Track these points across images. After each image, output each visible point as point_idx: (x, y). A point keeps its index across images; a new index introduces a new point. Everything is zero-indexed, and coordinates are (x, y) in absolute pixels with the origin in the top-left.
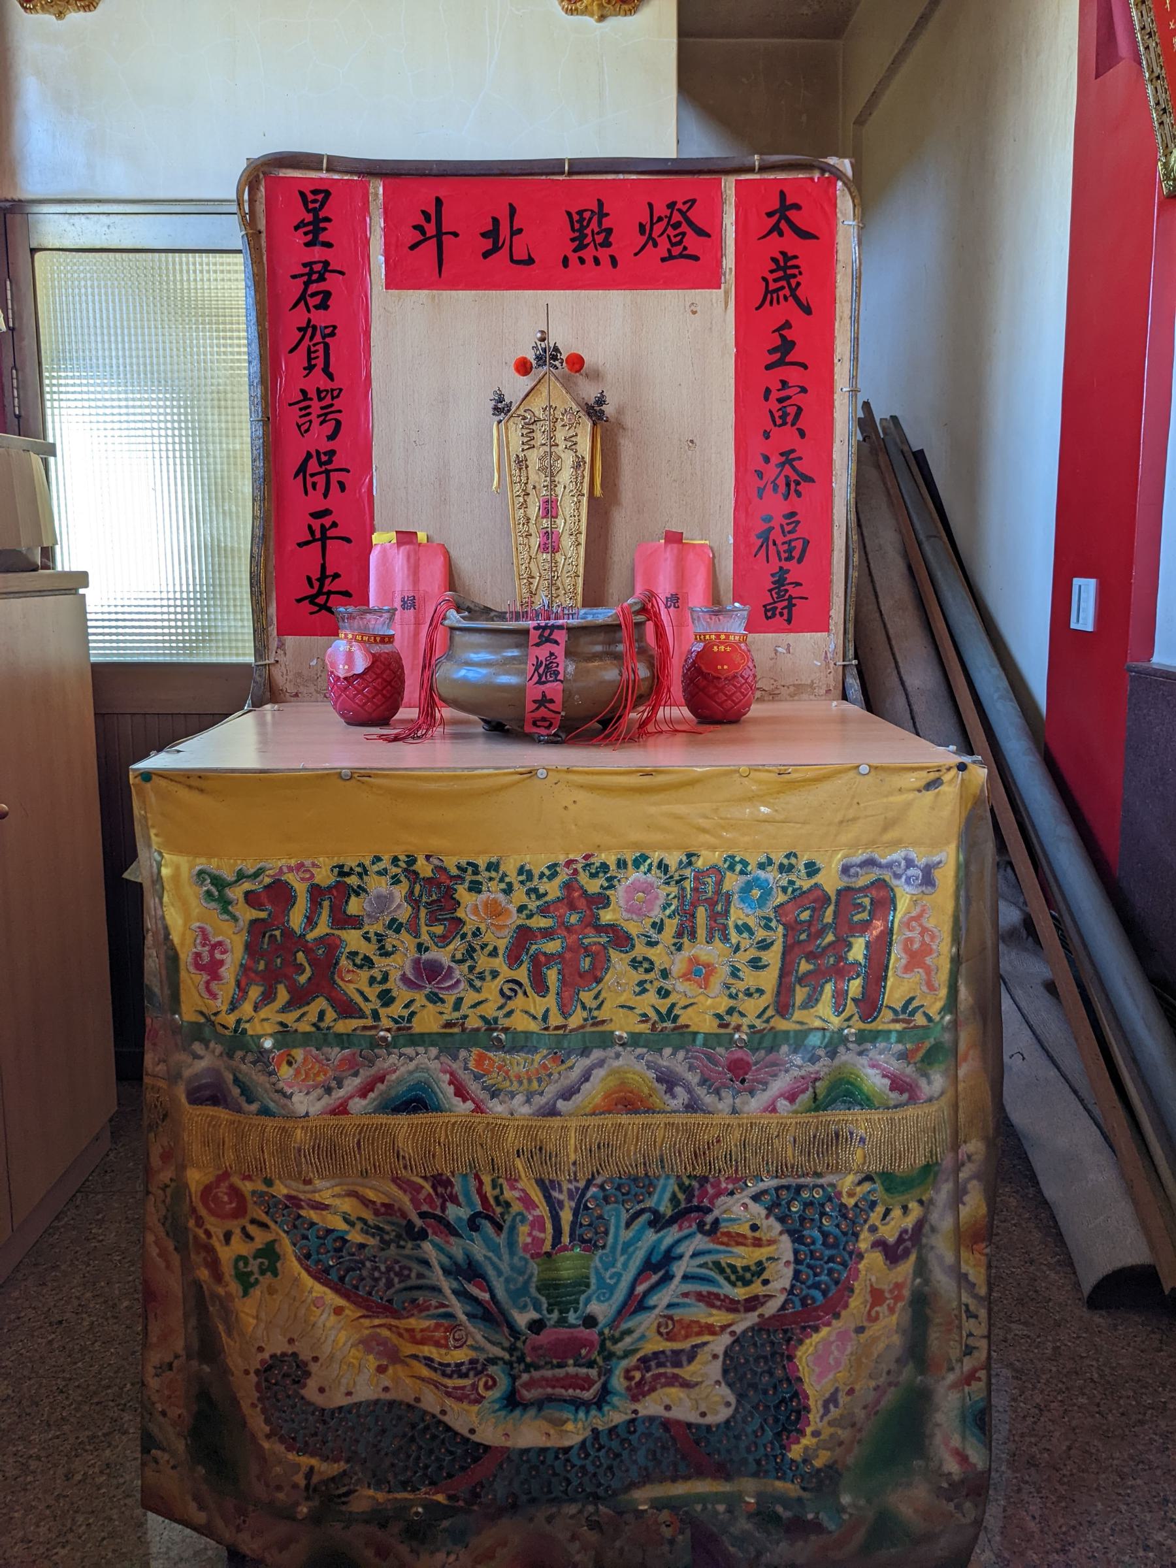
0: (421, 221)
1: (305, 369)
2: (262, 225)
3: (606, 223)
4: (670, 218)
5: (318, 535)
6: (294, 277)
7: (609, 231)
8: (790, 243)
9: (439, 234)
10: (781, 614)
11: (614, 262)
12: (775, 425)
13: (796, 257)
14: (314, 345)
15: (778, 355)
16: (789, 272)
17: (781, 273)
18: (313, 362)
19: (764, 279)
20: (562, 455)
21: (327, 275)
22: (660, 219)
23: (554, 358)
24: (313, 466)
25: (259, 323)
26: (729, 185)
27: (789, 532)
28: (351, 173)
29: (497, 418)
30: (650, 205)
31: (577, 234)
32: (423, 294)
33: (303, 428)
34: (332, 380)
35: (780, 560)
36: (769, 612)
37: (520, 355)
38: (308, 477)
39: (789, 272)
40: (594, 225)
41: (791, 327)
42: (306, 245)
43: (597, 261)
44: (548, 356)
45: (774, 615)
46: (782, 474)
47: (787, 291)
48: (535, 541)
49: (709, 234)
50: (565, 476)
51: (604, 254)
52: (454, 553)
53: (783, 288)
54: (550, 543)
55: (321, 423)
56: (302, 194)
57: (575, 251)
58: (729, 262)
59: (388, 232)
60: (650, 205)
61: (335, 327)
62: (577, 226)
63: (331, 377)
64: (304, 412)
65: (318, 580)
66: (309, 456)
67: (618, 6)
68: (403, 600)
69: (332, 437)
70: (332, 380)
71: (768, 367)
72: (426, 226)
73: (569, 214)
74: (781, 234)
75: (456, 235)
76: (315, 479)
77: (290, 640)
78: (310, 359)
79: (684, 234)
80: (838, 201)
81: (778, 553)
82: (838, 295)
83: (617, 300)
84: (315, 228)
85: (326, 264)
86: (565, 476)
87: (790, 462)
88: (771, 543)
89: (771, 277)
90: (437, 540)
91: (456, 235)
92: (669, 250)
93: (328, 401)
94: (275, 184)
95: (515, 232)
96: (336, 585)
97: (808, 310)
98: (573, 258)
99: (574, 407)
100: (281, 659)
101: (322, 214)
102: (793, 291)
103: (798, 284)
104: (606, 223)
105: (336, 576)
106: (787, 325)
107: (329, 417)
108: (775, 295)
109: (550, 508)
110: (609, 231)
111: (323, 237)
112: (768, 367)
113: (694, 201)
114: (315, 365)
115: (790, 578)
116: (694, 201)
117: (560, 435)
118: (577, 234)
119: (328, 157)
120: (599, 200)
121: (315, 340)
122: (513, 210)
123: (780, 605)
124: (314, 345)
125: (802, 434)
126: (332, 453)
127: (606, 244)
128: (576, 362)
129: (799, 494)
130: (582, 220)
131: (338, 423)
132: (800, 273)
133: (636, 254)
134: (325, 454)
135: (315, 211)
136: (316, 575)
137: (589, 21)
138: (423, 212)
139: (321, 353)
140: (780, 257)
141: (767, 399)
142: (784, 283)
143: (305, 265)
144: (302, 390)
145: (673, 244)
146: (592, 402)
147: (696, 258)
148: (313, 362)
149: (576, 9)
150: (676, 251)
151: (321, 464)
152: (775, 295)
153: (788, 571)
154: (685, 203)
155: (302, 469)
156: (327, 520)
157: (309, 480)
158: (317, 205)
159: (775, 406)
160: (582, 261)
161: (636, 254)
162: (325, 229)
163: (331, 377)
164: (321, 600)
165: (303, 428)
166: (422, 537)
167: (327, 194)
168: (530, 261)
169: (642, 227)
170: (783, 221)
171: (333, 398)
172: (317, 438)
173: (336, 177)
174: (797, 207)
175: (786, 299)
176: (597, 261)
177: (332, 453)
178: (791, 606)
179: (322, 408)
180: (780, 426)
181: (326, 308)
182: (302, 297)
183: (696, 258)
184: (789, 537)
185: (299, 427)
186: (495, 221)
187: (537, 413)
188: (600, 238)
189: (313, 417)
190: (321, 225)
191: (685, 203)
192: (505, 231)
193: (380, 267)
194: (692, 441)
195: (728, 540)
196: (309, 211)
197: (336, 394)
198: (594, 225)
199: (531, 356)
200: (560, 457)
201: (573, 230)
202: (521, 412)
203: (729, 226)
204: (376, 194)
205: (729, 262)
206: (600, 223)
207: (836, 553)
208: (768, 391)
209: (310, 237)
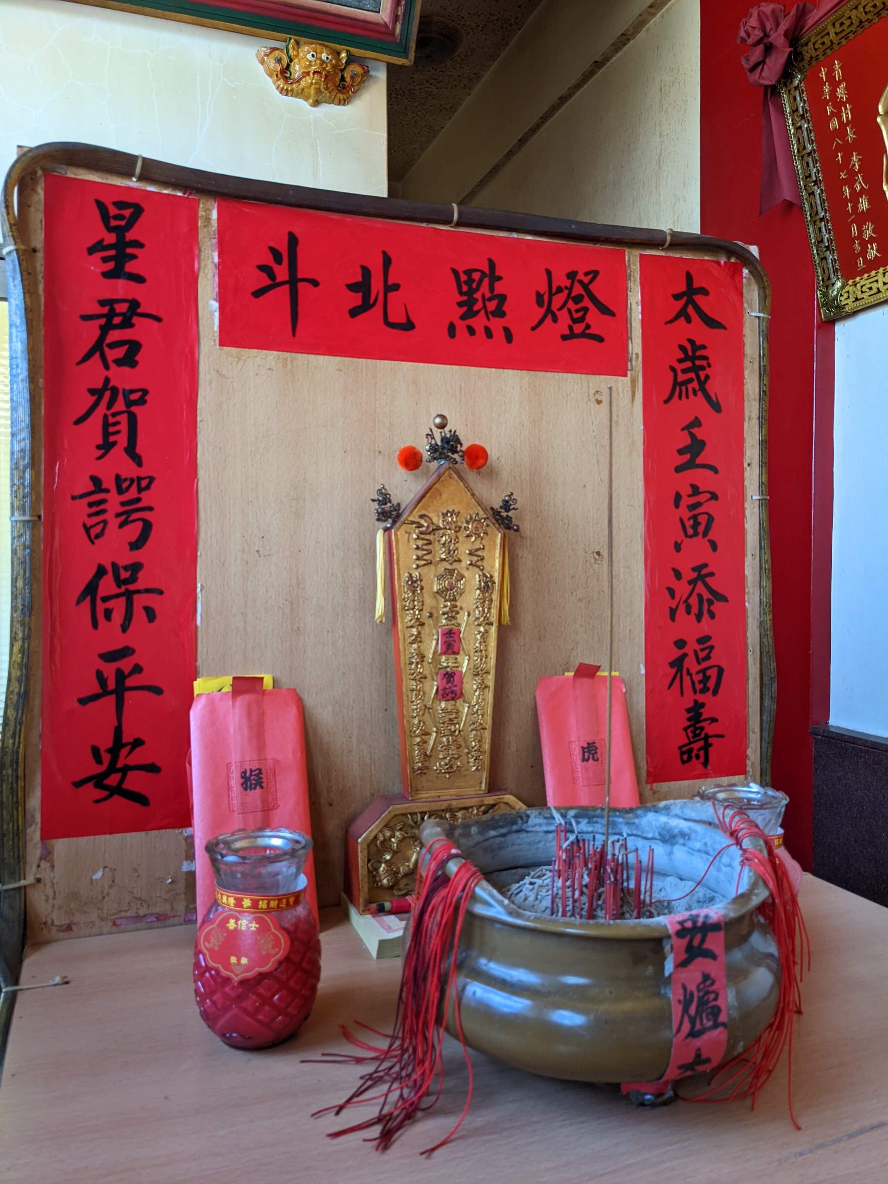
0: (269, 260)
1: (98, 447)
2: (38, 239)
3: (499, 288)
4: (571, 289)
5: (112, 685)
6: (86, 318)
7: (502, 298)
8: (697, 330)
9: (293, 282)
10: (698, 757)
11: (509, 337)
12: (686, 535)
13: (704, 347)
14: (114, 415)
15: (688, 456)
16: (697, 363)
17: (688, 364)
18: (112, 439)
19: (672, 369)
20: (466, 573)
21: (135, 320)
22: (560, 290)
23: (454, 450)
24: (107, 586)
25: (32, 378)
26: (633, 258)
27: (704, 659)
28: (175, 186)
29: (383, 525)
30: (548, 272)
31: (465, 298)
32: (271, 356)
33: (94, 532)
34: (140, 464)
35: (695, 692)
36: (686, 755)
37: (408, 444)
38: (99, 601)
39: (697, 363)
40: (485, 288)
41: (700, 425)
42: (105, 275)
43: (489, 333)
44: (448, 447)
45: (690, 759)
46: (695, 594)
47: (695, 384)
48: (432, 687)
49: (614, 311)
50: (470, 598)
51: (496, 324)
52: (309, 700)
53: (691, 380)
54: (451, 688)
55: (122, 525)
56: (100, 205)
57: (463, 318)
58: (636, 346)
59: (224, 270)
60: (548, 272)
61: (145, 392)
62: (465, 288)
63: (138, 460)
64: (95, 509)
65: (109, 751)
66: (101, 572)
67: (334, 93)
68: (243, 775)
69: (136, 545)
70: (140, 464)
71: (678, 469)
72: (277, 268)
73: (454, 271)
74: (689, 320)
75: (315, 283)
76: (110, 604)
77: (61, 846)
78: (106, 434)
79: (586, 310)
80: (745, 291)
81: (693, 683)
82: (746, 392)
83: (512, 381)
84: (119, 256)
85: (134, 304)
86: (470, 598)
87: (702, 578)
88: (685, 672)
89: (679, 367)
90: (287, 683)
91: (315, 283)
92: (570, 327)
93: (133, 493)
94: (58, 189)
95: (391, 288)
96: (139, 757)
97: (717, 407)
98: (461, 326)
99: (481, 513)
100: (46, 875)
101: (130, 236)
102: (702, 384)
103: (707, 377)
104: (499, 288)
105: (138, 743)
106: (697, 423)
107: (135, 516)
108: (684, 388)
109: (451, 642)
110: (502, 298)
111: (131, 267)
112: (678, 469)
113: (596, 273)
114: (115, 443)
115: (706, 713)
116: (596, 273)
117: (464, 549)
118: (465, 298)
119: (144, 159)
120: (490, 260)
121: (115, 409)
122: (387, 261)
123: (696, 746)
124: (114, 415)
125: (714, 546)
126: (136, 568)
127: (499, 313)
128: (477, 457)
129: (712, 615)
130: (470, 281)
131: (147, 526)
132: (709, 365)
133: (533, 329)
134: (126, 568)
135: (120, 231)
136: (106, 742)
137: (303, 105)
138: (272, 249)
139: (124, 427)
140: (688, 346)
141: (677, 505)
142: (693, 375)
143: (102, 303)
144: (92, 478)
145: (575, 321)
146: (497, 506)
147: (601, 339)
148: (112, 439)
149: (292, 90)
150: (578, 328)
151: (119, 582)
152: (684, 388)
153: (703, 705)
154: (586, 274)
155: (91, 590)
156: (126, 664)
157: (101, 607)
158: (123, 223)
159: (686, 514)
160: (471, 331)
161: (533, 329)
162: (134, 257)
163: (138, 460)
164: (113, 780)
165: (94, 532)
166: (268, 683)
167: (138, 210)
168: (409, 326)
169: (539, 296)
170: (690, 306)
171: (140, 490)
172: (115, 546)
173: (151, 188)
174: (704, 291)
175: (695, 394)
176: (489, 333)
177: (136, 568)
178: (706, 747)
179: (123, 504)
180: (691, 537)
181: (133, 364)
182: (98, 347)
183: (601, 339)
184: (705, 665)
185: (87, 529)
186: (366, 271)
187: (435, 520)
188: (492, 306)
189: (109, 516)
190: (129, 250)
191: (586, 274)
192: (377, 286)
193: (212, 315)
194: (598, 553)
195: (639, 670)
196: (110, 229)
197: (144, 484)
198: (485, 288)
199: (424, 448)
200: (462, 577)
201: (461, 293)
202: (414, 517)
203: (634, 307)
204: (208, 219)
205: (636, 346)
206: (492, 289)
207: (751, 681)
208: (678, 497)
209: (111, 265)
